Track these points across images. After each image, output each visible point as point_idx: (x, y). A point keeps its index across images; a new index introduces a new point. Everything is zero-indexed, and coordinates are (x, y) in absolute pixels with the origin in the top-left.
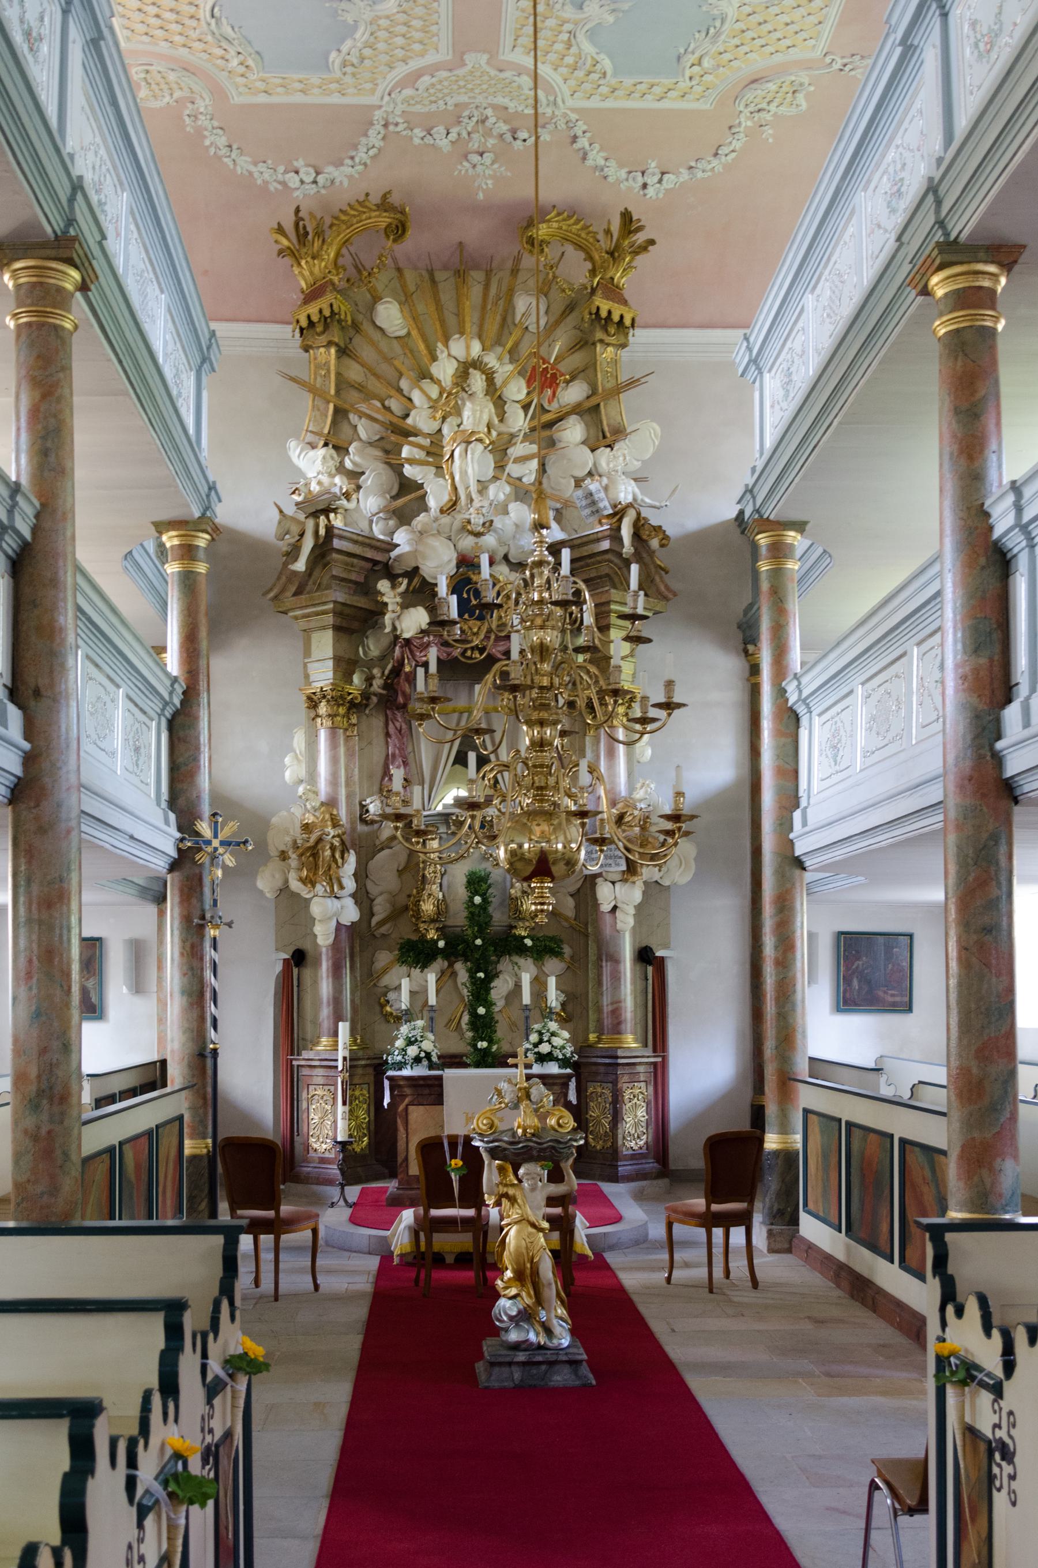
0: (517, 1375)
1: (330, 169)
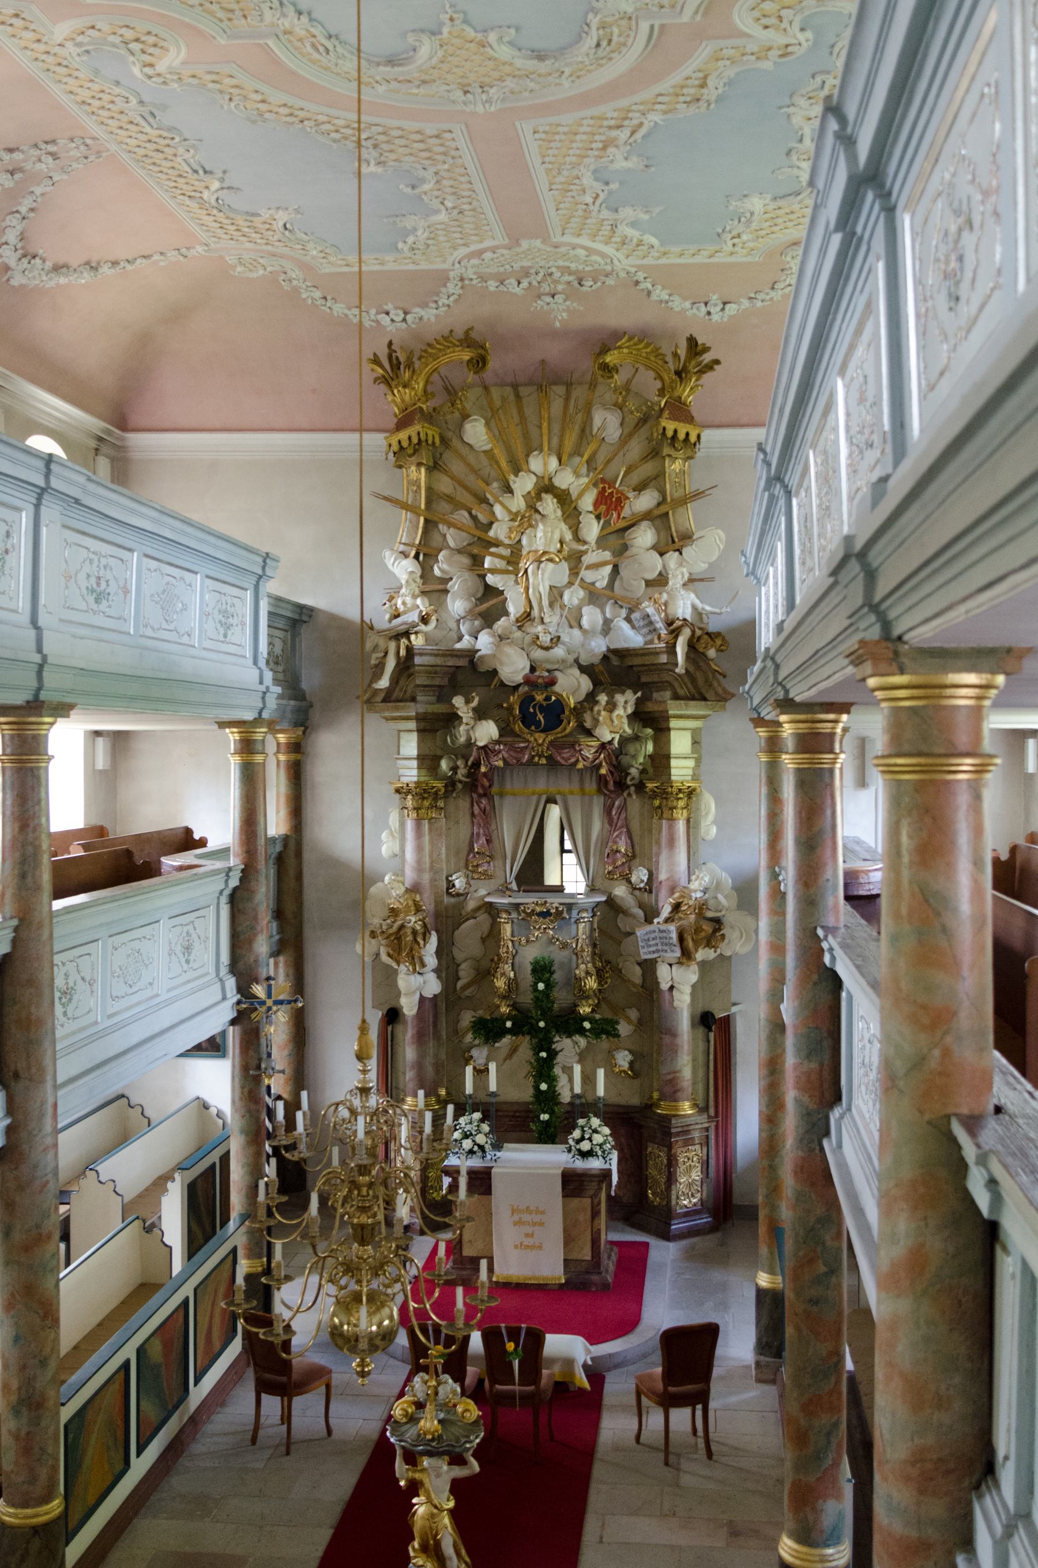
1: (417, 310)
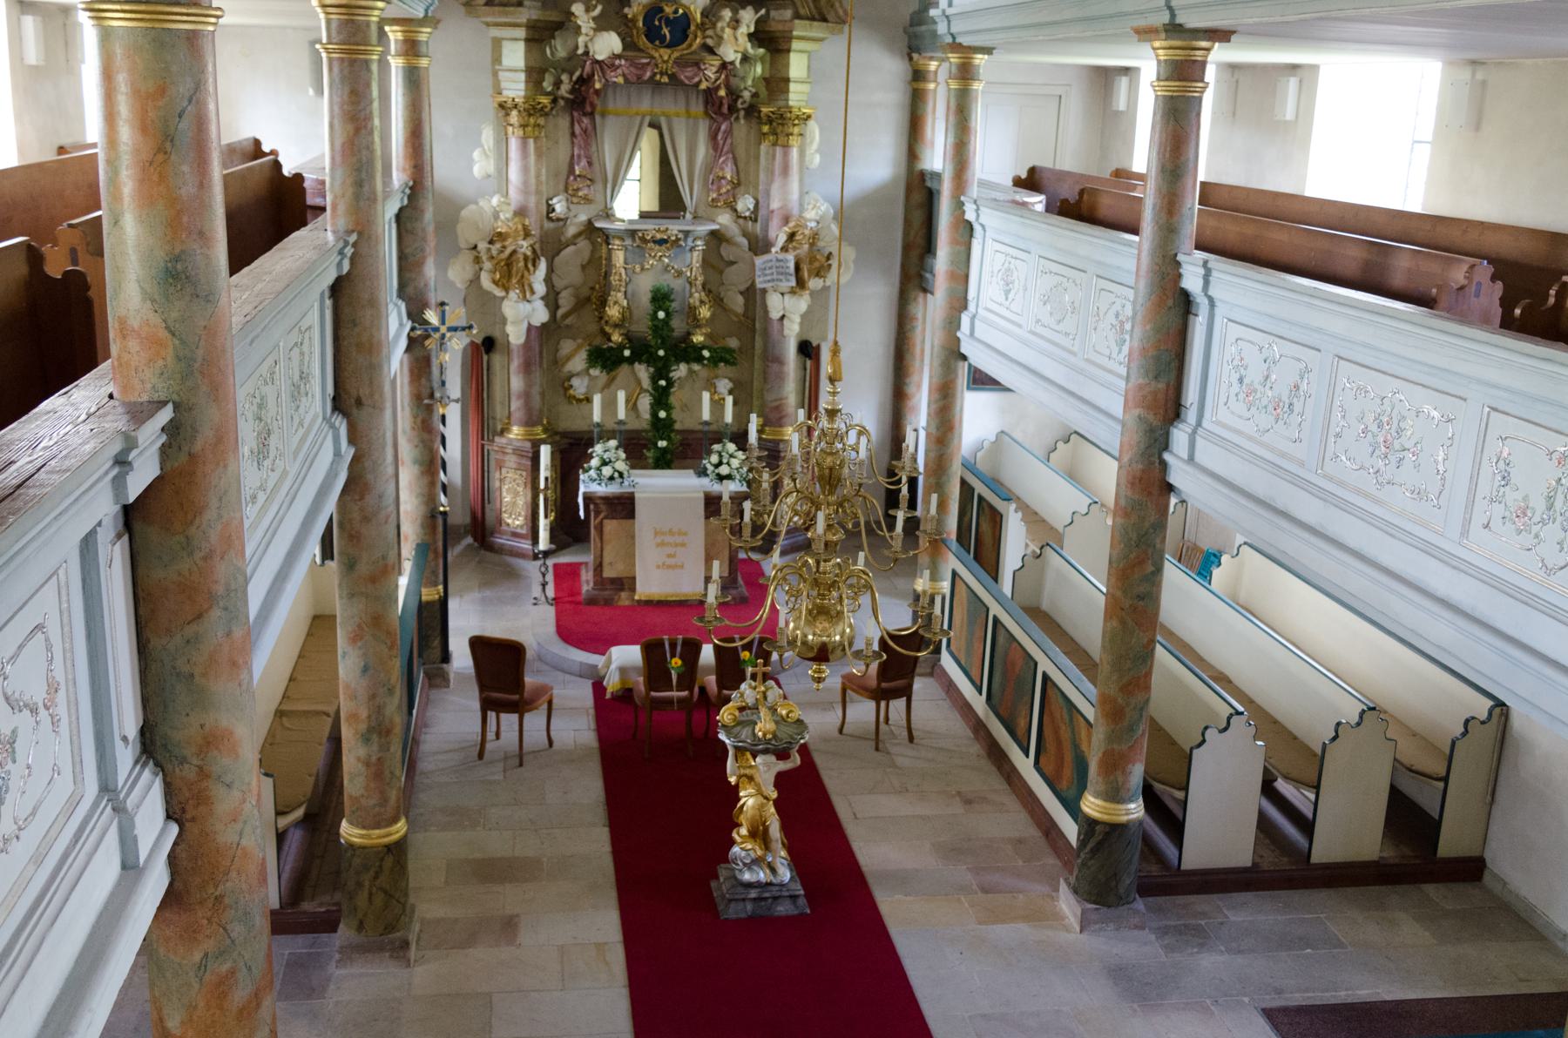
0: (749, 907)
